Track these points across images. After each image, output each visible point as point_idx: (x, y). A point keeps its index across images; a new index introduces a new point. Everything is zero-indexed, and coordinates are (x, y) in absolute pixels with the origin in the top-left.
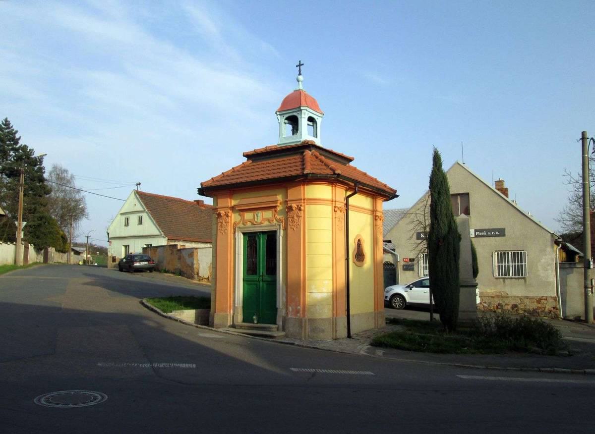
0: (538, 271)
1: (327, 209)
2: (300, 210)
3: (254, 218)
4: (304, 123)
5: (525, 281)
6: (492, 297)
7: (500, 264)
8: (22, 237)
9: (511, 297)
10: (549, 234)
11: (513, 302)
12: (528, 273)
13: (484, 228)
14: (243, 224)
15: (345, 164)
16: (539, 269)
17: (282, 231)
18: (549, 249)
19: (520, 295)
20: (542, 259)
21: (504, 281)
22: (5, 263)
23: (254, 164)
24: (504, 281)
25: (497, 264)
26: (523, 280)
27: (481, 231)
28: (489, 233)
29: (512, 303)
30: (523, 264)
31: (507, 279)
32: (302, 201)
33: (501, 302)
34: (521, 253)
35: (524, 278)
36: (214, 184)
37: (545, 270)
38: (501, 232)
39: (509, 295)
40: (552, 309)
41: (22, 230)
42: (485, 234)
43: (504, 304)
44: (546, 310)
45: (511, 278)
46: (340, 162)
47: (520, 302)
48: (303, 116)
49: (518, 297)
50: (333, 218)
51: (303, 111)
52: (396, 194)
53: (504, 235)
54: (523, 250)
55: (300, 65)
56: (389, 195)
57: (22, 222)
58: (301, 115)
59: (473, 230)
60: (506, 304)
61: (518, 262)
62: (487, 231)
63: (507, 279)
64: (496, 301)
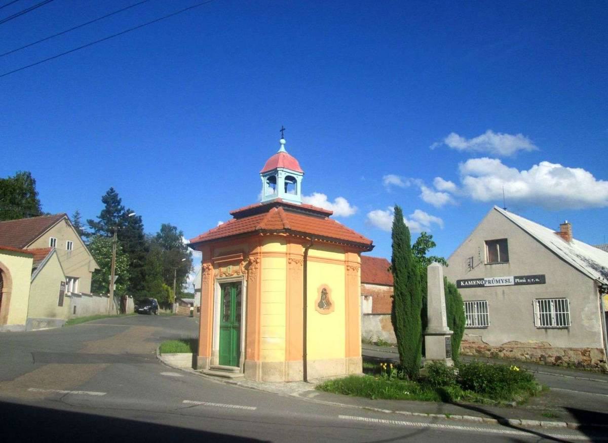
0: (583, 320)
1: (282, 262)
2: (257, 263)
3: (227, 270)
4: (281, 181)
5: (569, 331)
6: (534, 348)
7: (479, 314)
8: (115, 289)
9: (554, 348)
10: (592, 281)
11: (556, 354)
12: (571, 322)
13: (523, 275)
14: (220, 276)
15: (324, 218)
16: (583, 318)
17: (245, 281)
18: (592, 297)
19: (564, 347)
20: (585, 307)
21: (546, 331)
22: (96, 313)
23: (239, 221)
24: (546, 331)
25: (538, 313)
26: (566, 331)
27: (521, 278)
28: (529, 280)
29: (555, 355)
30: (565, 312)
31: (549, 328)
32: (259, 254)
33: (544, 354)
34: (563, 301)
35: (567, 328)
36: (201, 240)
37: (589, 319)
38: (541, 279)
39: (552, 346)
40: (599, 362)
41: (115, 283)
42: (525, 281)
43: (547, 356)
44: (593, 363)
45: (553, 328)
46: (318, 217)
47: (564, 354)
48: (279, 176)
49: (561, 348)
50: (289, 270)
51: (279, 172)
52: (373, 245)
53: (544, 283)
54: (565, 298)
55: (283, 130)
56: (370, 247)
57: (114, 276)
58: (278, 175)
59: (513, 277)
60: (550, 356)
61: (546, 311)
62: (527, 277)
63: (549, 328)
64: (539, 353)
